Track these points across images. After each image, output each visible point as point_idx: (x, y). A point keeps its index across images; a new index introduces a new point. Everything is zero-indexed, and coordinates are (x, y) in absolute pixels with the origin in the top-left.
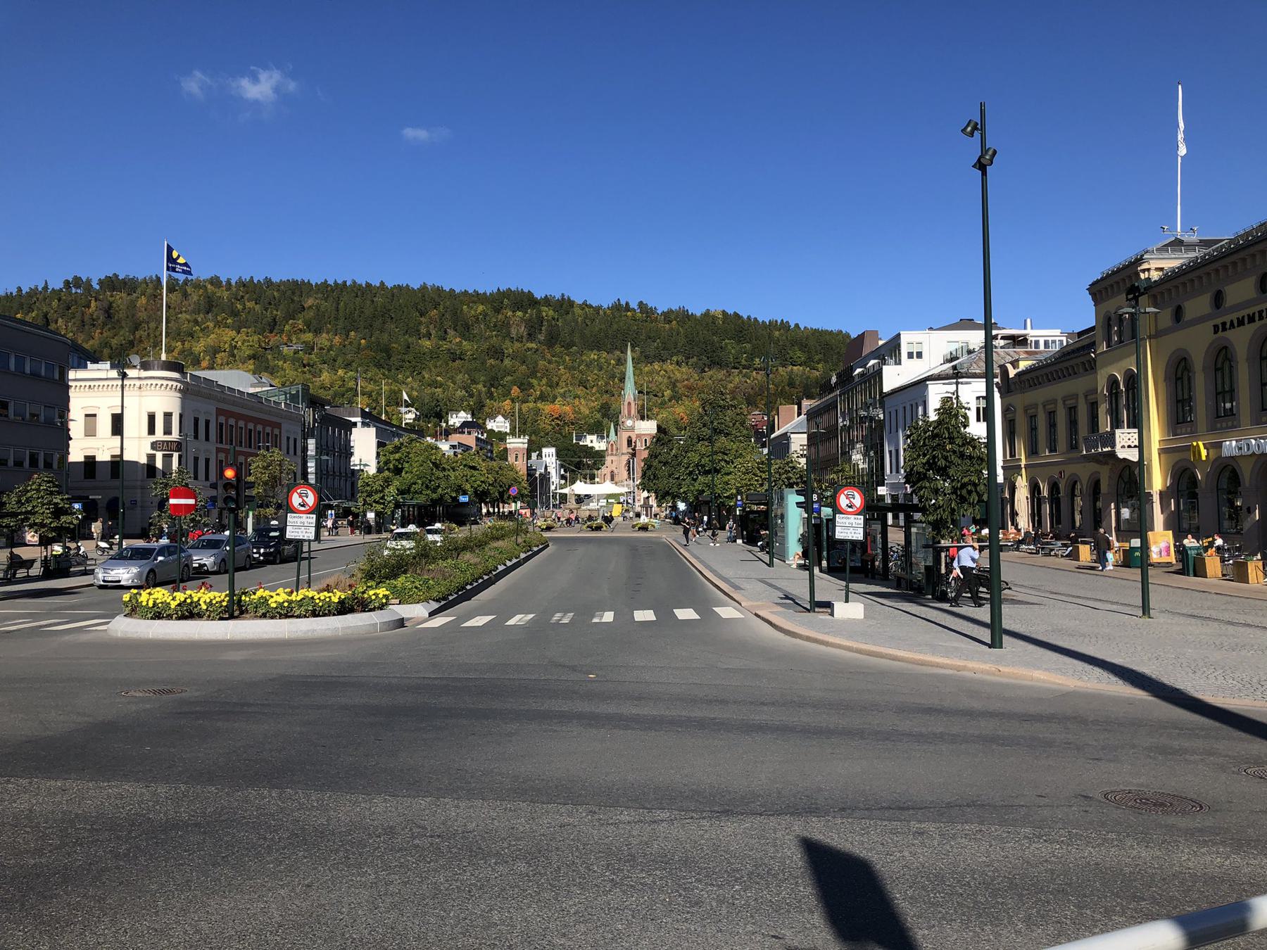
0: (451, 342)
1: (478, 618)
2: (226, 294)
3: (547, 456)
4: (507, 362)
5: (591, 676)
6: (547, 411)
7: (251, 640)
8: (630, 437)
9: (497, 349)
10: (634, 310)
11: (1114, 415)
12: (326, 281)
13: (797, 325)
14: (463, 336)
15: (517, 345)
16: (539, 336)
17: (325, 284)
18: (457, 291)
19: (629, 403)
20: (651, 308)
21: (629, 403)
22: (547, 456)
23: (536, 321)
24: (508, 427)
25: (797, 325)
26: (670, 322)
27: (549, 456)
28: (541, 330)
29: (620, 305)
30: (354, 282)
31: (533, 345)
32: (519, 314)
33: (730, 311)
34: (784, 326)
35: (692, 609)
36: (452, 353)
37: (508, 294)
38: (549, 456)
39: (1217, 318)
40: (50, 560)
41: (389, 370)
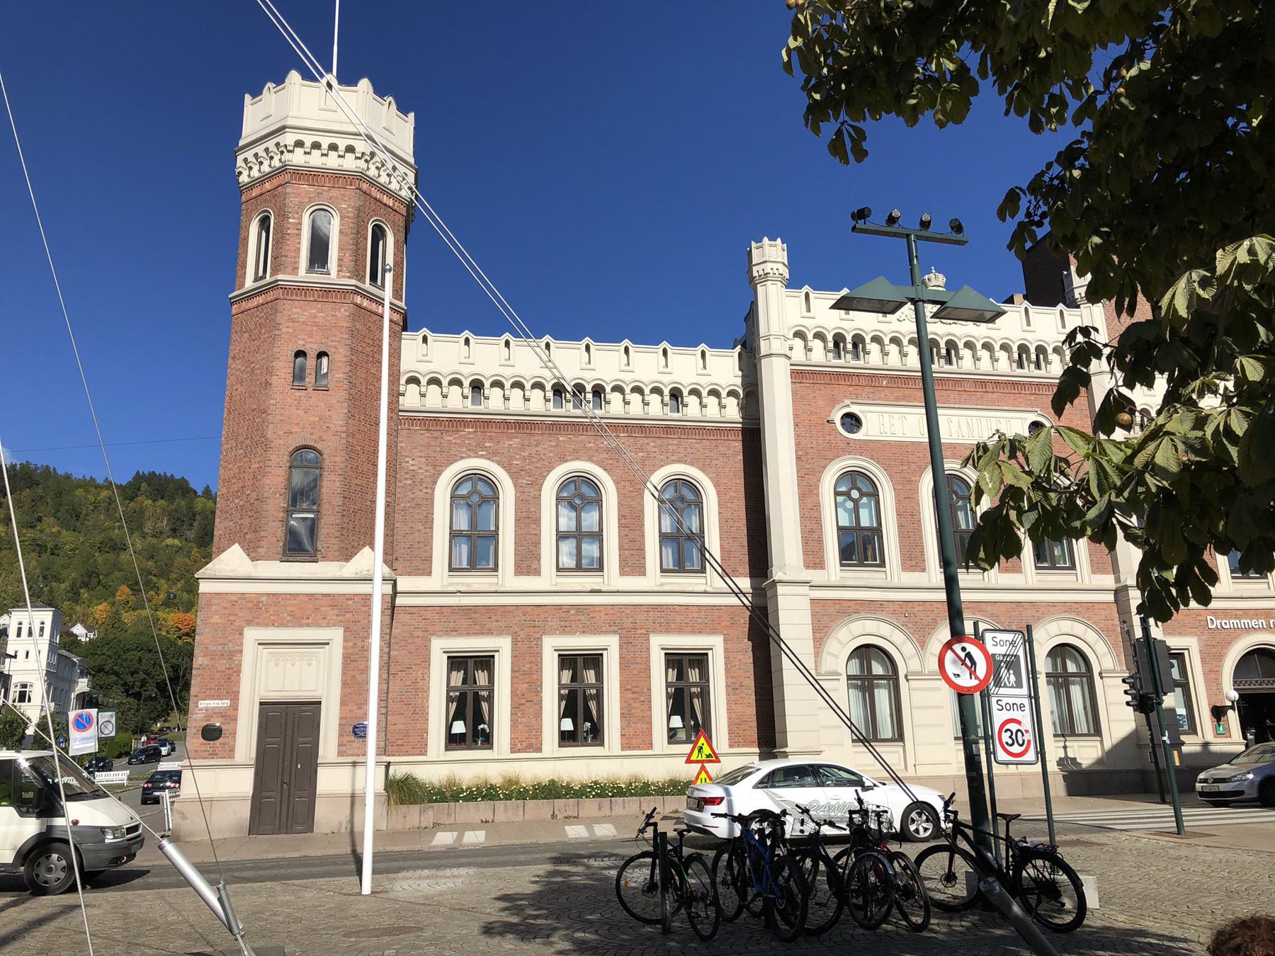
0: (42, 531)
3: (25, 632)
5: (1196, 569)
6: (171, 623)
9: (116, 544)
11: (401, 864)
14: (65, 525)
16: (188, 533)
22: (25, 632)
23: (185, 512)
27: (30, 634)
28: (192, 525)
31: (176, 542)
32: (162, 502)
35: (1250, 379)
36: (38, 545)
37: (152, 478)
38: (30, 634)
39: (460, 865)
40: (750, 877)
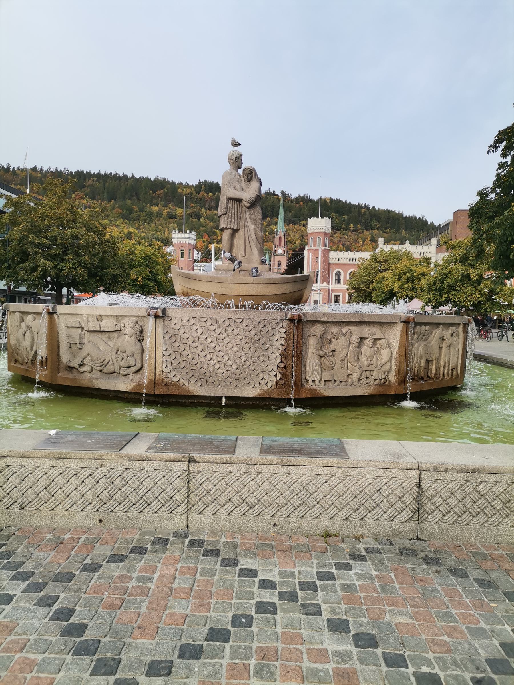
0: (170, 208)
1: (414, 678)
2: (39, 175)
4: (202, 220)
7: (84, 398)
8: (279, 261)
10: (278, 195)
12: (100, 171)
13: (374, 207)
15: (208, 212)
17: (99, 174)
18: (176, 182)
19: (280, 238)
20: (288, 194)
21: (280, 238)
24: (200, 257)
25: (374, 207)
26: (299, 202)
29: (270, 192)
30: (116, 174)
33: (334, 198)
34: (366, 207)
41: (130, 221)
